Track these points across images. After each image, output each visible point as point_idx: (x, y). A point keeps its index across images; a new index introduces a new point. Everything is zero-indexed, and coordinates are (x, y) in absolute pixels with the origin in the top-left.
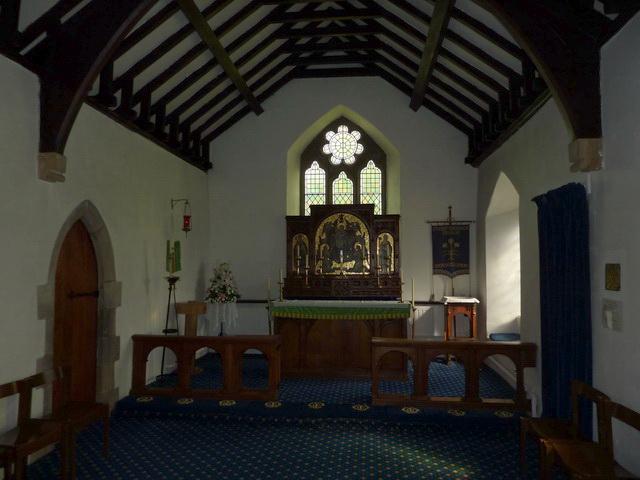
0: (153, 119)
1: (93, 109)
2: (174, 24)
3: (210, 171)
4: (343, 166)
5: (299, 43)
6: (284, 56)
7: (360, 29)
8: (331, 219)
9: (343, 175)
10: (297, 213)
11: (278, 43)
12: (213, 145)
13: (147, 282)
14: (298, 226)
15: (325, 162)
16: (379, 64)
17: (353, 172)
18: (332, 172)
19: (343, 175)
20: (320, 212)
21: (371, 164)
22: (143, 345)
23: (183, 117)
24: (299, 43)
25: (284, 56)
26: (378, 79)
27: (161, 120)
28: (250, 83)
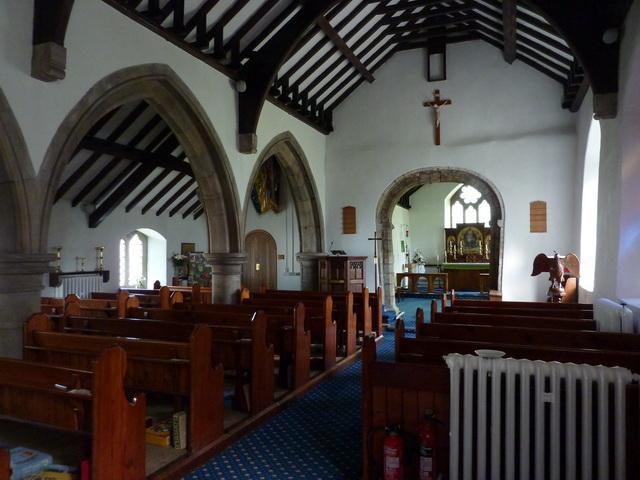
0: (291, 96)
1: (317, 132)
2: (318, 37)
3: (331, 133)
4: (471, 204)
5: (399, 26)
6: (383, 28)
7: (464, 18)
8: (465, 230)
9: (471, 207)
10: (449, 227)
11: (378, 18)
12: (336, 113)
13: (624, 304)
14: (450, 232)
15: (462, 201)
16: (476, 10)
17: (476, 206)
18: (466, 206)
19: (471, 207)
20: (461, 227)
21: (485, 202)
22: (400, 277)
23: (319, 100)
24: (399, 26)
25: (383, 28)
26: (481, 41)
27: (287, 90)
28: (363, 60)
